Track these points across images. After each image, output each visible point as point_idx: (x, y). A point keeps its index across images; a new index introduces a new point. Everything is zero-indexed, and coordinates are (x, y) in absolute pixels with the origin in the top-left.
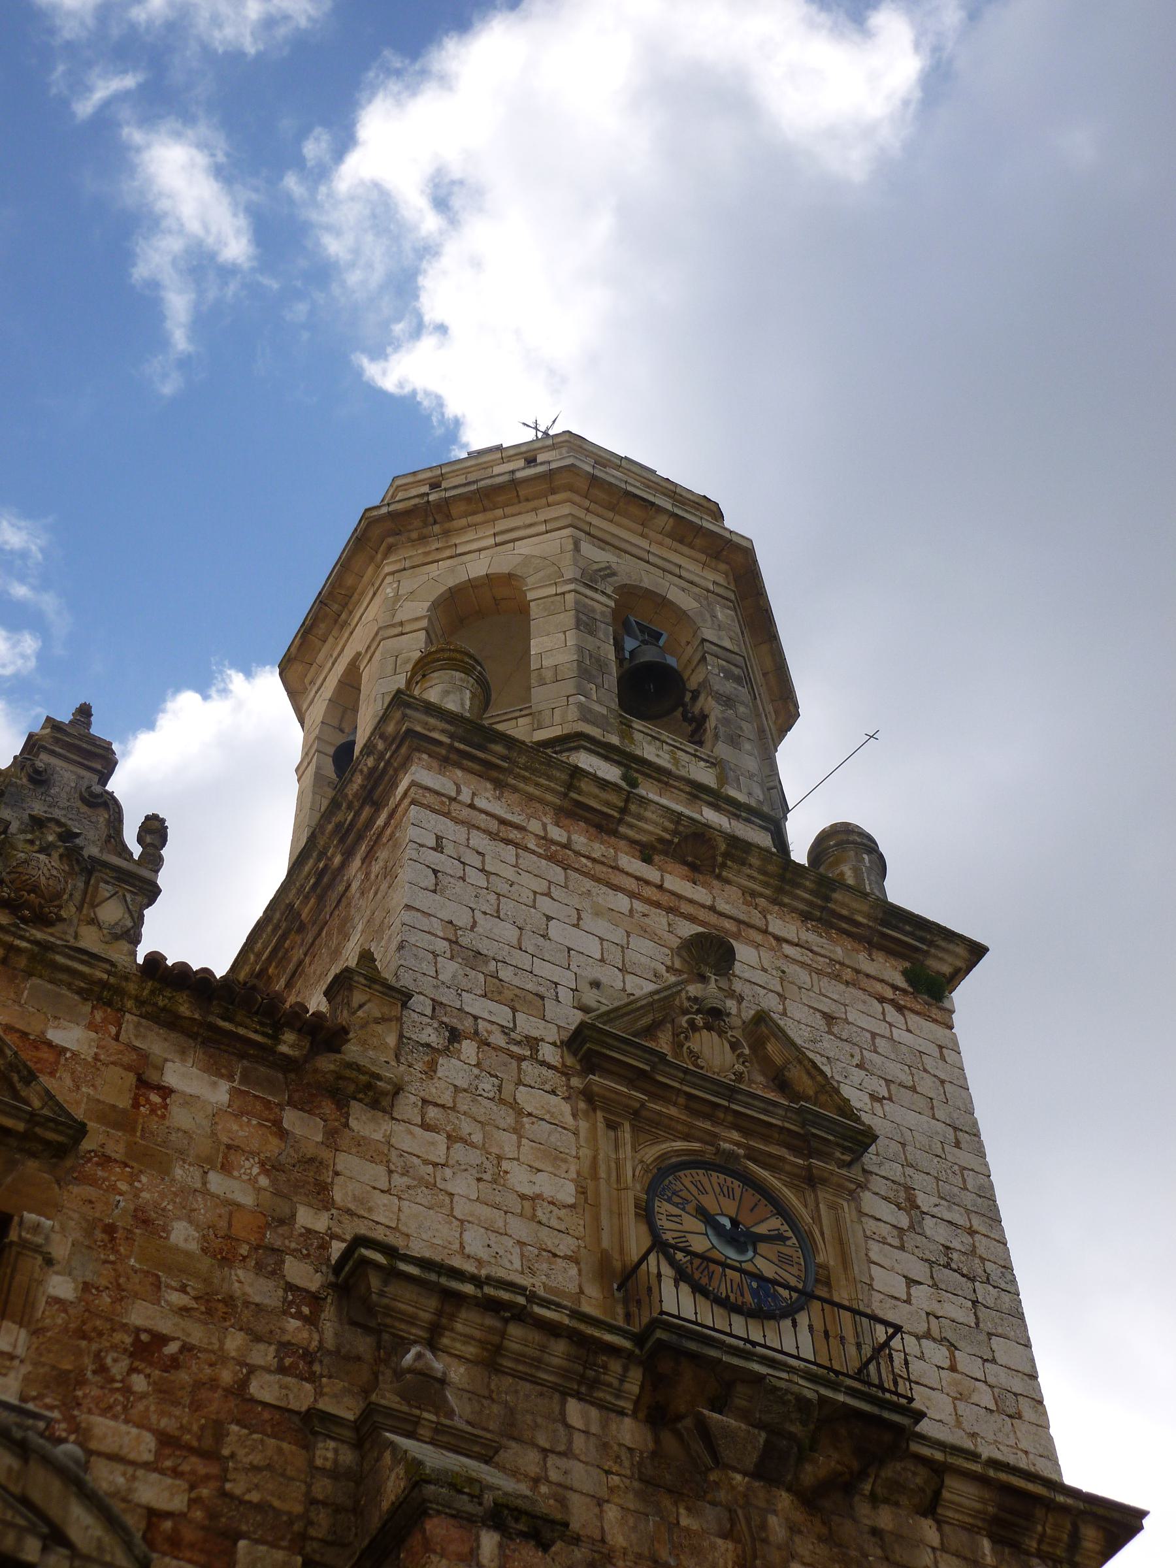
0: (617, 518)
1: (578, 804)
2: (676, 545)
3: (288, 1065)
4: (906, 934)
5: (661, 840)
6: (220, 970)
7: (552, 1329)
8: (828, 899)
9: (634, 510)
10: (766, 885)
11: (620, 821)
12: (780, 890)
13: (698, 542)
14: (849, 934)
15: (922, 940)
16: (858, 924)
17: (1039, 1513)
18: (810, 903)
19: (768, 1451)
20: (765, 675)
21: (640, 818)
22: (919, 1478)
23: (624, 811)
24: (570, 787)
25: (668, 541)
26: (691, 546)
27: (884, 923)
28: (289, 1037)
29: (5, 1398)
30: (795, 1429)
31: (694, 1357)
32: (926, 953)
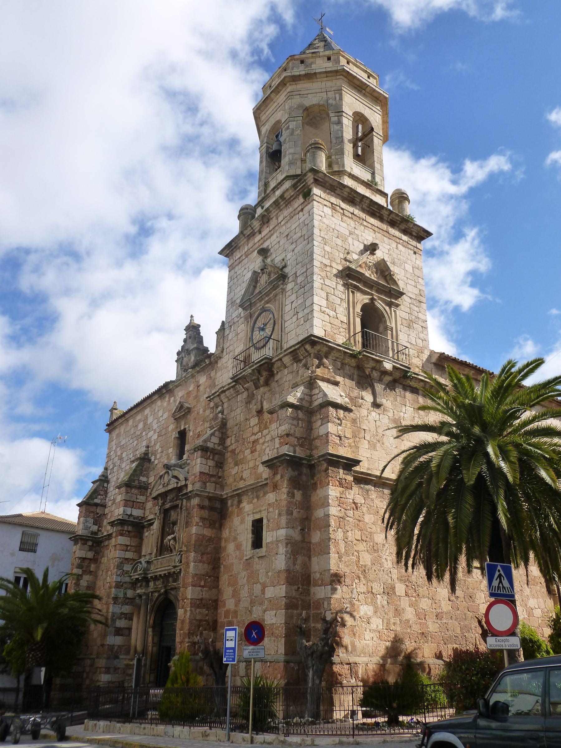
0: (269, 106)
1: (248, 236)
2: (279, 95)
3: (211, 363)
4: (300, 185)
5: (260, 225)
6: (174, 378)
7: (229, 389)
8: (285, 198)
9: (268, 101)
10: (277, 210)
11: (254, 230)
12: (279, 208)
13: (280, 88)
14: (294, 199)
15: (303, 182)
16: (293, 196)
17: (298, 351)
18: (285, 203)
19: (255, 384)
20: (327, 77)
21: (255, 226)
22: (279, 364)
23: (252, 228)
24: (244, 235)
25: (278, 96)
26: (281, 90)
27: (295, 189)
28: (206, 361)
29: (5, 576)
30: (254, 378)
31: (238, 379)
32: (306, 183)
